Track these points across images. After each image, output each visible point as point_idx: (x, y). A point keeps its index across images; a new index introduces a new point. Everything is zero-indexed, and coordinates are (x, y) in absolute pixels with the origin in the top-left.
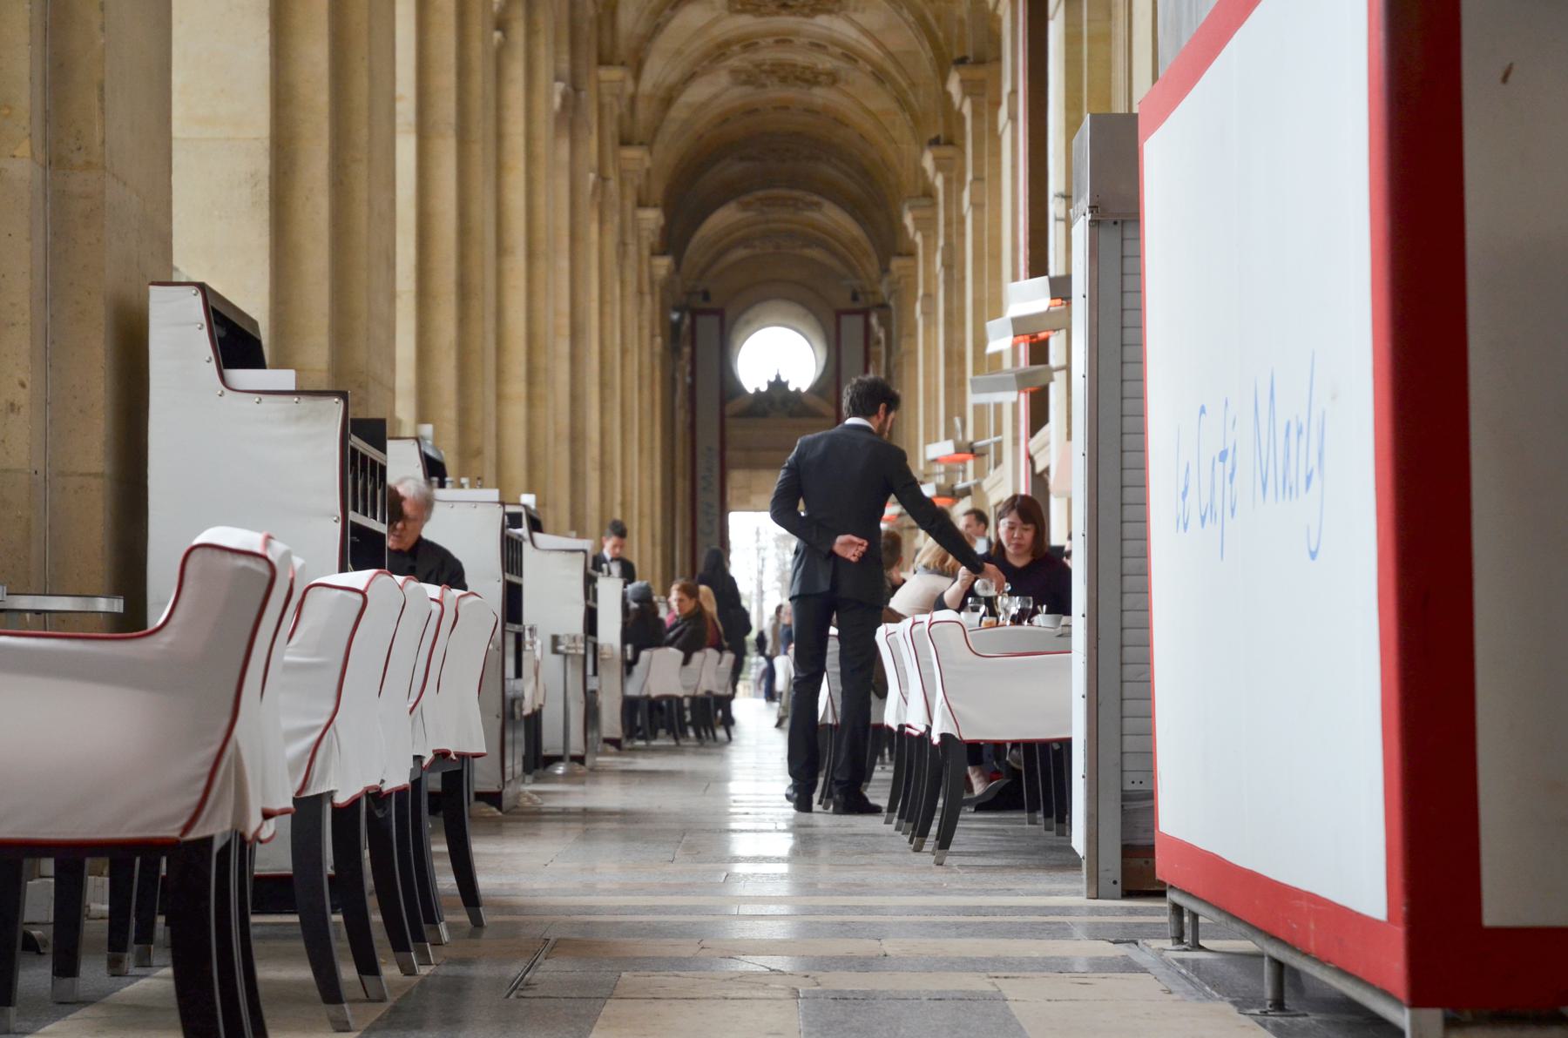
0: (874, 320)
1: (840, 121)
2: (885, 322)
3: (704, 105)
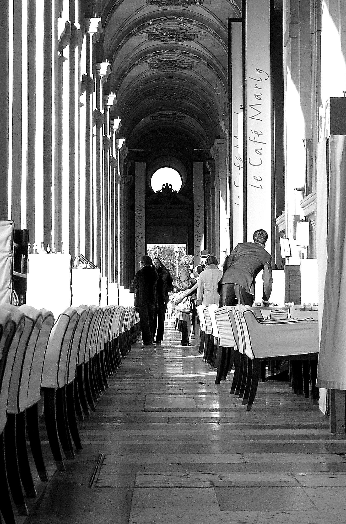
0: (207, 164)
1: (194, 83)
2: (213, 165)
3: (137, 77)
